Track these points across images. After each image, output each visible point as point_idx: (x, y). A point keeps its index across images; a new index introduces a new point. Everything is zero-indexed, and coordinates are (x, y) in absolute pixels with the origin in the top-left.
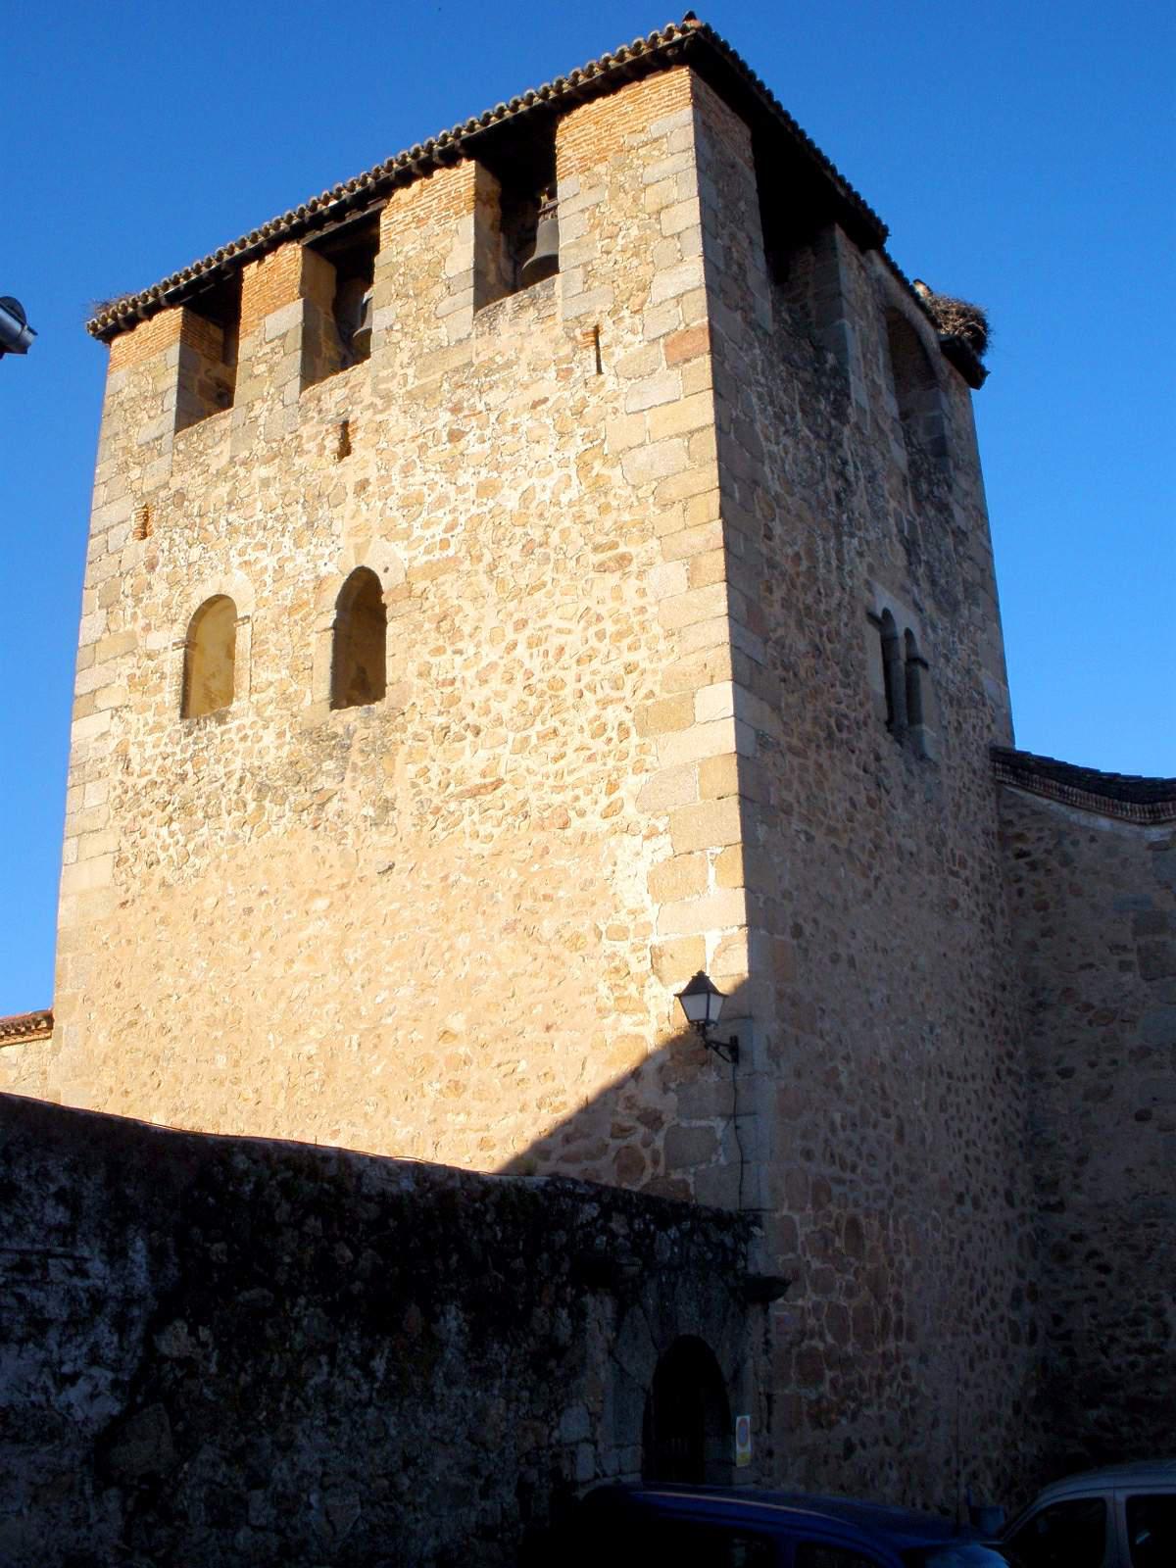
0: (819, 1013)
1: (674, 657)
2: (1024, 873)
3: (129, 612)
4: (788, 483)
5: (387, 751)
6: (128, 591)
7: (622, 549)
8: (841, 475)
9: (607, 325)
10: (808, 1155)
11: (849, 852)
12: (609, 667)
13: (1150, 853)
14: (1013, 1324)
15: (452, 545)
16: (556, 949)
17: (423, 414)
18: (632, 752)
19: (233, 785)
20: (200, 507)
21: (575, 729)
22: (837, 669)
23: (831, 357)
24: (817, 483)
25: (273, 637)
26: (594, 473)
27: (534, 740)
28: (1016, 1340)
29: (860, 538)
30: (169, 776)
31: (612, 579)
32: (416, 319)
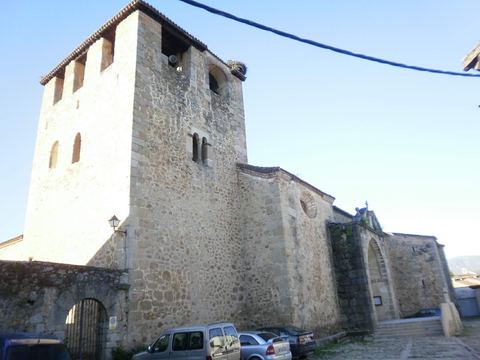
2: (243, 192)
13: (269, 185)
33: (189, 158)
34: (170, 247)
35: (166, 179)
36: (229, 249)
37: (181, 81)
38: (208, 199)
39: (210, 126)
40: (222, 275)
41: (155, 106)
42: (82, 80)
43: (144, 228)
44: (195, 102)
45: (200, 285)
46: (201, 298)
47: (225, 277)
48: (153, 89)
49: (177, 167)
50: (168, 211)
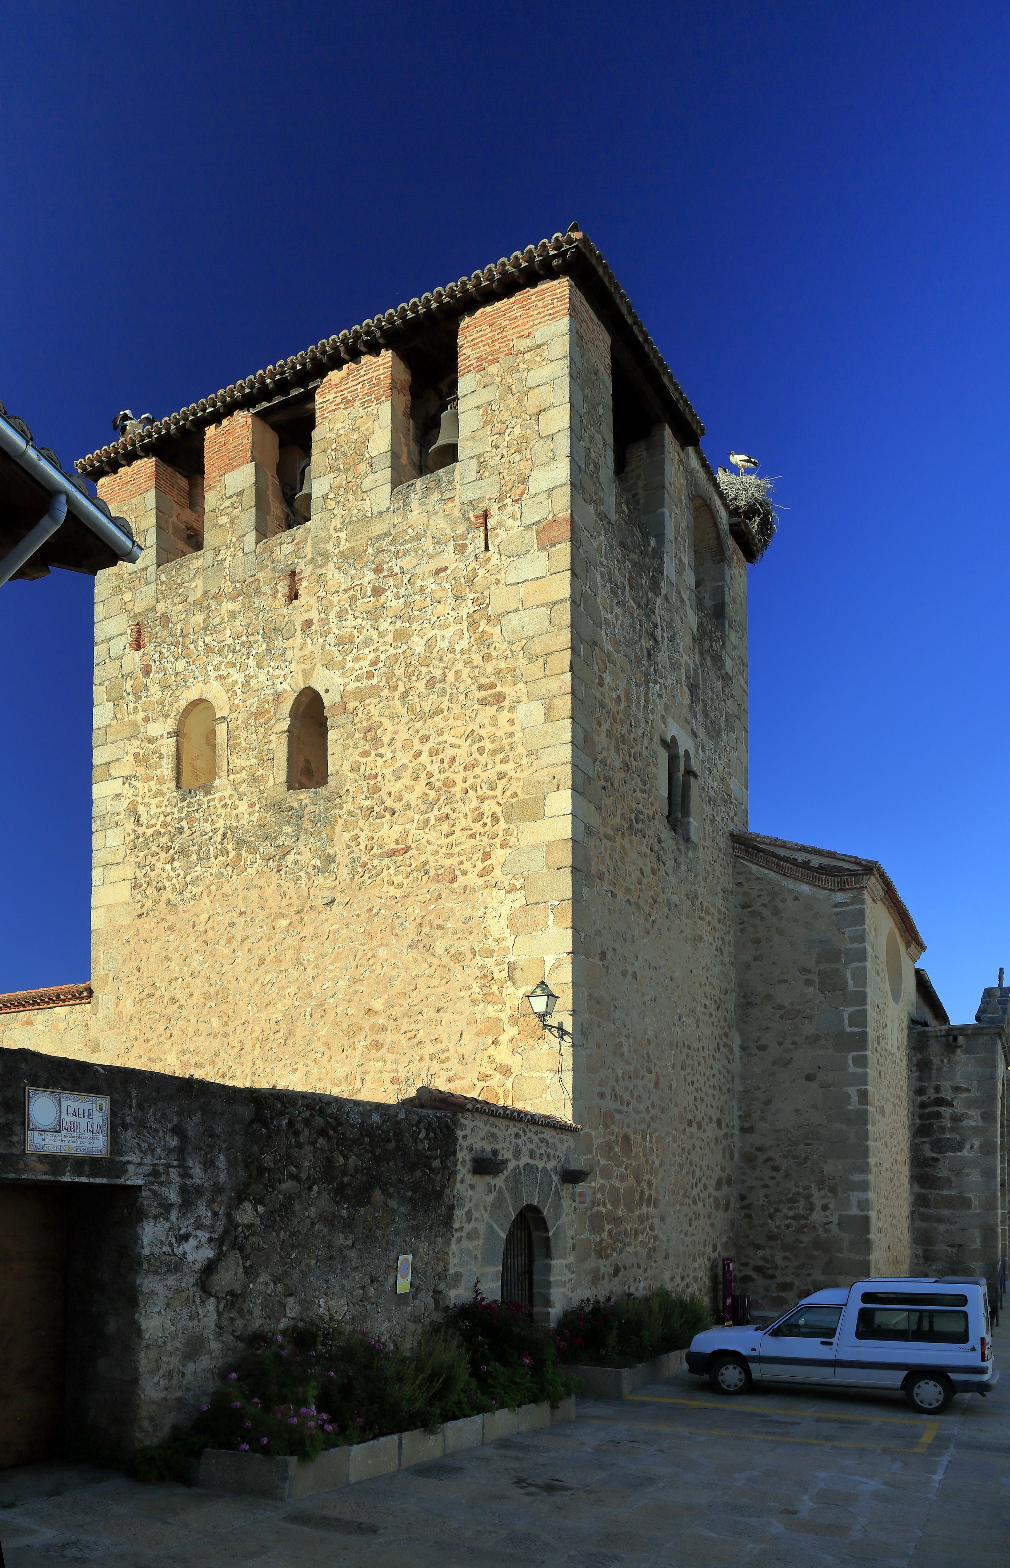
0: (613, 1008)
1: (532, 770)
3: (131, 705)
4: (617, 643)
5: (330, 822)
6: (130, 690)
7: (499, 689)
8: (652, 636)
9: (494, 509)
10: (602, 1096)
11: (637, 904)
12: (487, 774)
14: (716, 1199)
15: (375, 676)
16: (445, 960)
17: (352, 572)
18: (501, 833)
19: (218, 838)
20: (182, 629)
21: (461, 815)
22: (638, 780)
23: (653, 542)
24: (636, 643)
25: (243, 734)
26: (480, 630)
27: (432, 821)
28: (717, 1207)
29: (661, 684)
30: (170, 828)
31: (491, 711)
32: (346, 491)
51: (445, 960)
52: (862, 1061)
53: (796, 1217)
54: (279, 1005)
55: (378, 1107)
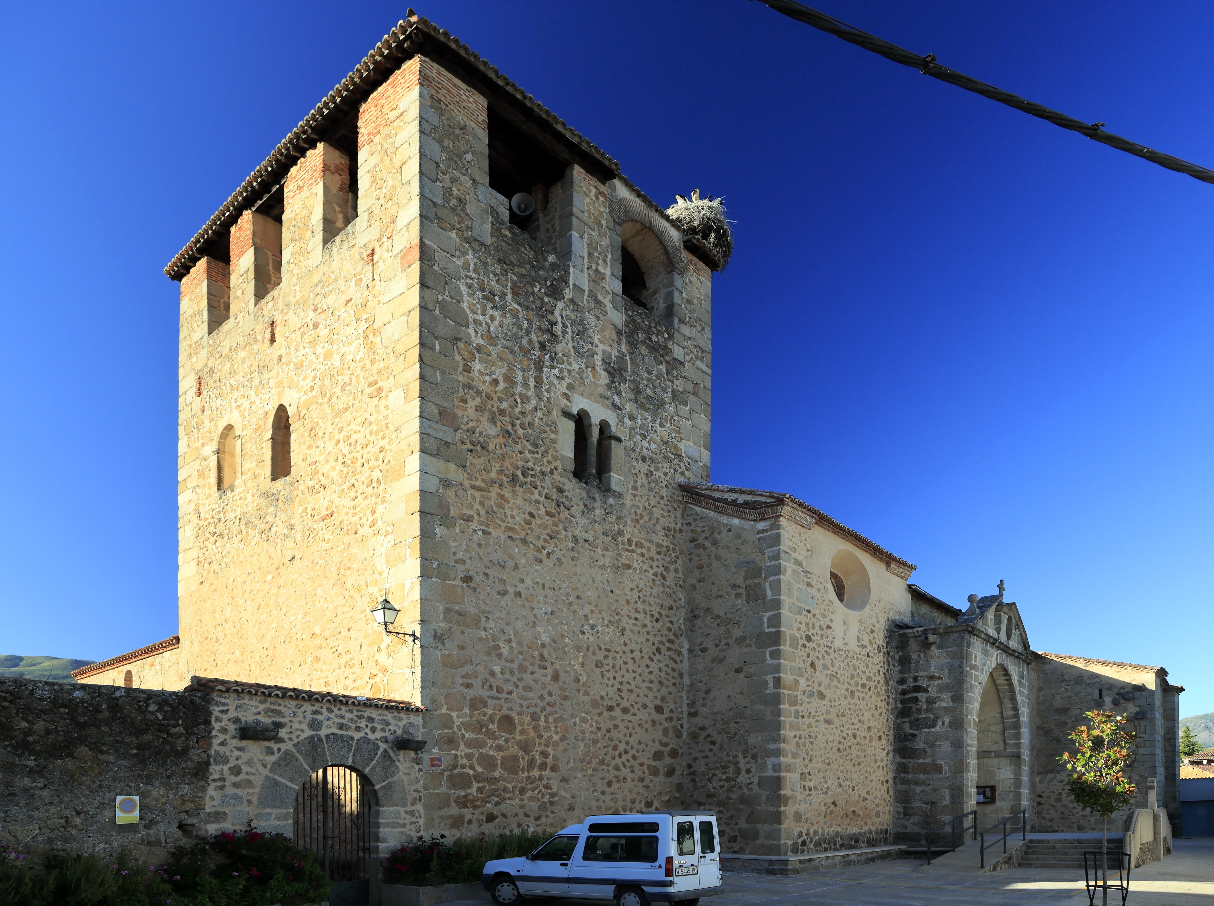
2: (693, 550)
12: (373, 450)
17: (302, 314)
31: (375, 401)
33: (565, 471)
34: (515, 666)
35: (509, 519)
36: (651, 673)
37: (547, 271)
38: (607, 564)
39: (619, 394)
40: (630, 725)
41: (477, 341)
42: (278, 265)
43: (455, 627)
44: (581, 330)
45: (581, 745)
46: (582, 770)
47: (638, 729)
48: (469, 295)
49: (536, 491)
50: (511, 590)
51: (352, 592)
52: (777, 655)
53: (728, 780)
54: (268, 637)
55: (175, 693)
